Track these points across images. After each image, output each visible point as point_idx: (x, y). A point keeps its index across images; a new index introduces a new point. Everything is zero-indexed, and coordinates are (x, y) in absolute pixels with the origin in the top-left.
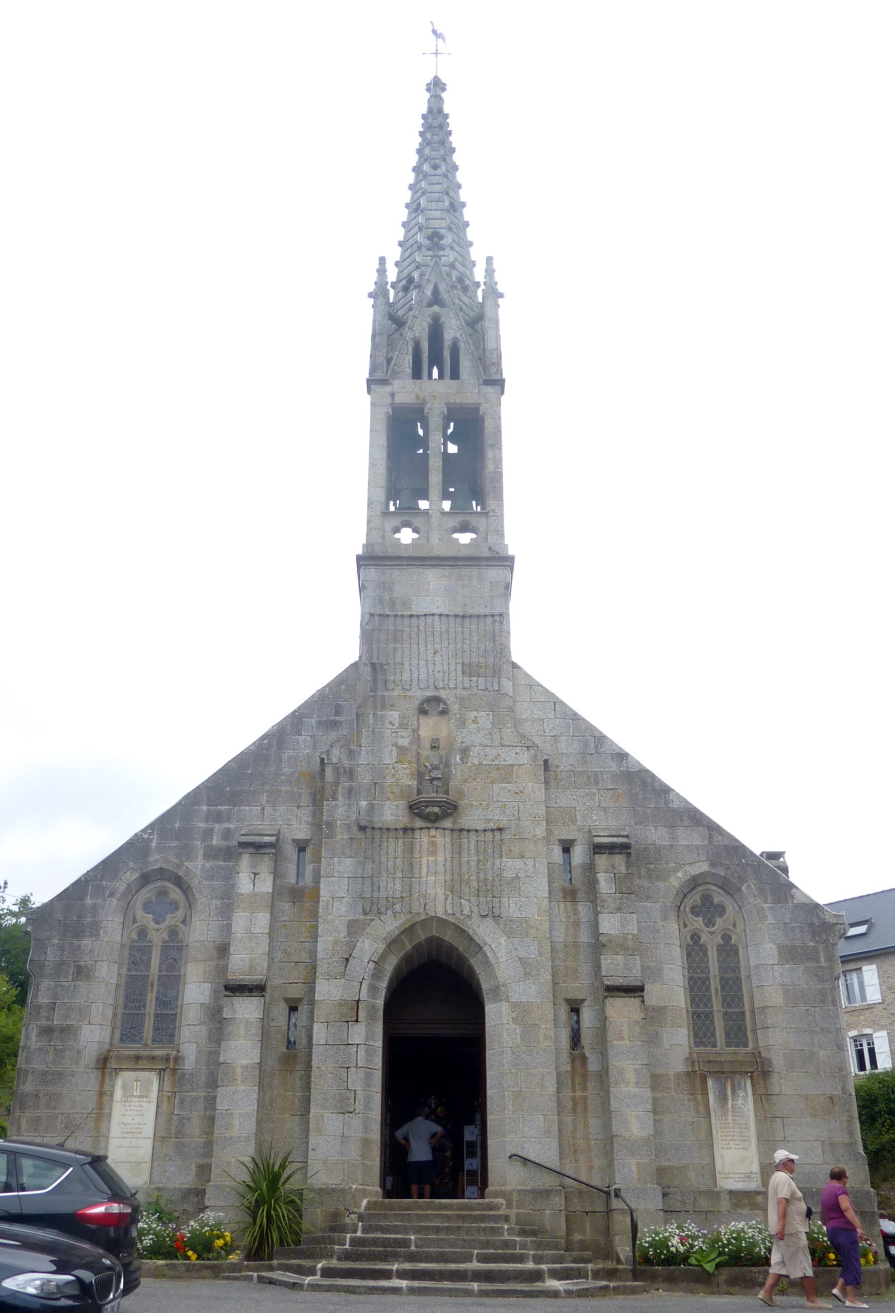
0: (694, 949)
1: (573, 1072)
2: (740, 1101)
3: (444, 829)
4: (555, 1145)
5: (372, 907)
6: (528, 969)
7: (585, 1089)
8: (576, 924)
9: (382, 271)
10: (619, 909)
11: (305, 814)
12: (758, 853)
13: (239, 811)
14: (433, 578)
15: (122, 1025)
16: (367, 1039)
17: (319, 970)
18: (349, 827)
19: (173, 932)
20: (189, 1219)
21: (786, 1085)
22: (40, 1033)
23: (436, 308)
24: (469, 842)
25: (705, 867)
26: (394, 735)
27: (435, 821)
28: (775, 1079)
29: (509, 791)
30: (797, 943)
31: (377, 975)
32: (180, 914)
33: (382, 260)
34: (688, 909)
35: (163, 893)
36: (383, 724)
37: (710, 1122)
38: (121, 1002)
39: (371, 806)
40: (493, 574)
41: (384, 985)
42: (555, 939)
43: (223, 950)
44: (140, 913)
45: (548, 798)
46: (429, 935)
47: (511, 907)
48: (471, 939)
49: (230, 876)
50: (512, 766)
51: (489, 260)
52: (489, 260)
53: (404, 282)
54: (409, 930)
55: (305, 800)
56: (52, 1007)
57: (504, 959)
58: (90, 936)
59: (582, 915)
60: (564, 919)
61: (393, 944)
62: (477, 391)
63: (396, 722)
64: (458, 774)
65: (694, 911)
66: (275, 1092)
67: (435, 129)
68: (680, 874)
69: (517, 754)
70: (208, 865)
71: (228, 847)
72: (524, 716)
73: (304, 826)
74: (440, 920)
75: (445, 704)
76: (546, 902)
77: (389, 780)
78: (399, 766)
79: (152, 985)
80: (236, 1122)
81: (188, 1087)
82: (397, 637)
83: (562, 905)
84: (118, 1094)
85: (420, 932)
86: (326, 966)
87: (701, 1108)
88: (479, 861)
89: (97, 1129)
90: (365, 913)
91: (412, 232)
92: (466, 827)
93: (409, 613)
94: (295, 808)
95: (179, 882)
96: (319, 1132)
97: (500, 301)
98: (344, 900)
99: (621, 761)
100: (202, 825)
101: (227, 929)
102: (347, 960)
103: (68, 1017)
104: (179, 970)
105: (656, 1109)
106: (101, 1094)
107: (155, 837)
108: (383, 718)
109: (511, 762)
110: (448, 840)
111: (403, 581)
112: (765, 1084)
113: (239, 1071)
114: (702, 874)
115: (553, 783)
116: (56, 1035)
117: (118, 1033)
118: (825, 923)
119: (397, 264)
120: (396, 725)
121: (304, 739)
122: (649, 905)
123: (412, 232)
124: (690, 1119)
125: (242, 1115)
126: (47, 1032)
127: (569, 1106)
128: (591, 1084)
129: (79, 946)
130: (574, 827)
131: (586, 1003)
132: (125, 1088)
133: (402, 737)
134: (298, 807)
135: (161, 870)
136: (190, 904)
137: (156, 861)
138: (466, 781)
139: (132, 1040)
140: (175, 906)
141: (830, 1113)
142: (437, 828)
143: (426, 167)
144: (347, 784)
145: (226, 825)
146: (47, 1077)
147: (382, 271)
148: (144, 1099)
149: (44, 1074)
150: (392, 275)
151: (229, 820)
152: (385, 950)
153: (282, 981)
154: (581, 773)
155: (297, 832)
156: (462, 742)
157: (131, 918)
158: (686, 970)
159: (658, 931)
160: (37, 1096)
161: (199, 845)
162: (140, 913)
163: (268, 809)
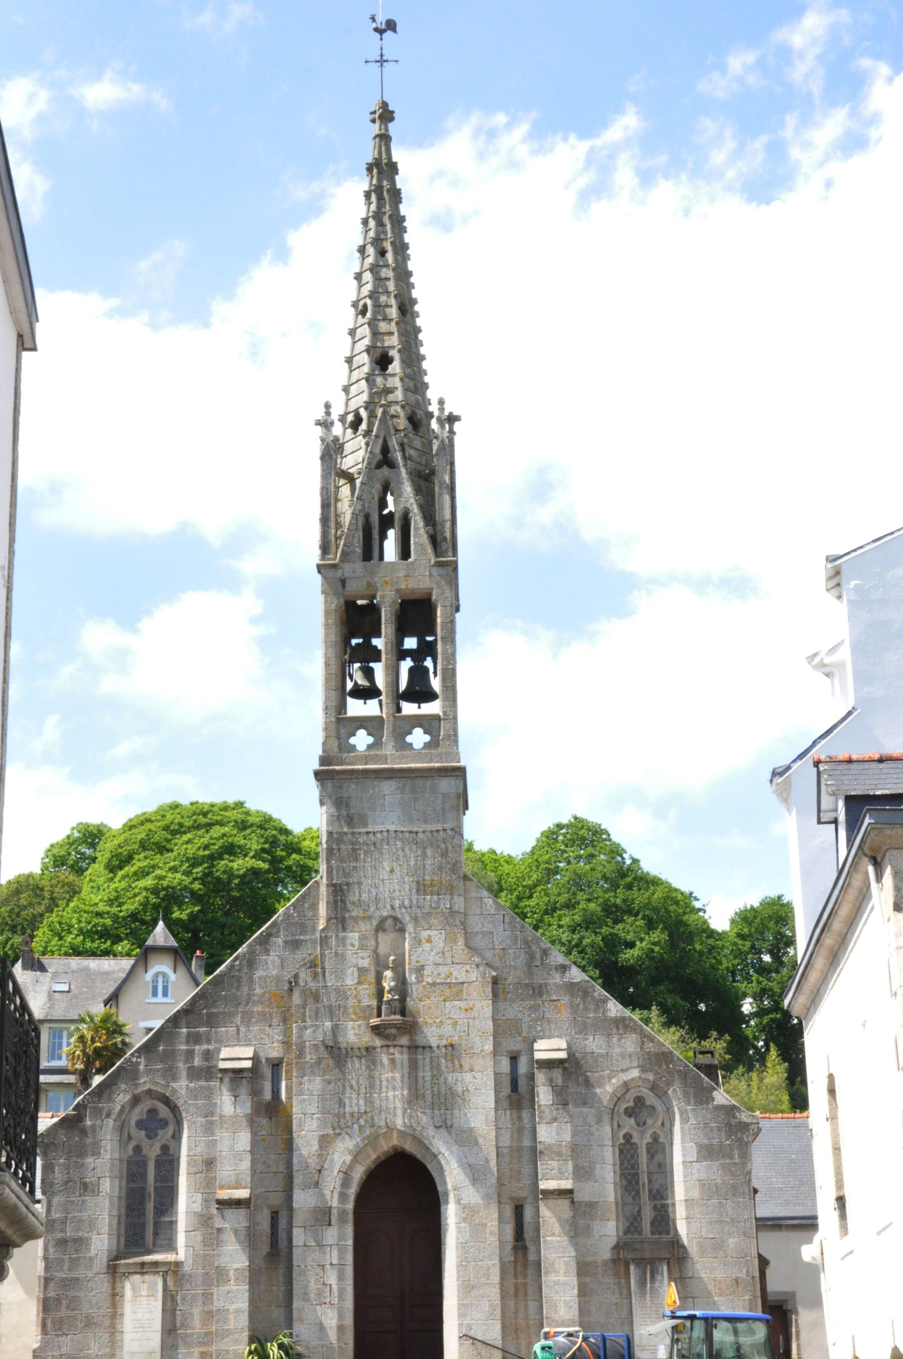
0: (627, 1151)
1: (515, 1261)
2: (657, 1284)
3: (402, 1046)
4: (498, 1327)
5: (338, 1123)
7: (525, 1276)
8: (520, 1131)
10: (555, 1119)
13: (216, 1032)
15: (126, 1232)
16: (339, 1240)
17: (296, 1181)
19: (165, 1148)
20: (690, 1025)
22: (56, 1244)
23: (385, 470)
24: (424, 1059)
26: (355, 956)
29: (460, 1008)
30: (715, 1142)
32: (170, 1130)
34: (622, 1110)
35: (153, 1112)
37: (631, 1302)
38: (123, 1211)
40: (446, 785)
41: (353, 1191)
42: (501, 1144)
43: (210, 1163)
44: (134, 1131)
45: (495, 1011)
46: (391, 1145)
48: (428, 1149)
49: (209, 1094)
50: (463, 983)
51: (441, 402)
53: (350, 417)
56: (64, 1222)
58: (93, 1155)
59: (526, 1121)
60: (510, 1126)
62: (428, 573)
63: (357, 944)
65: (629, 1113)
66: (263, 1287)
68: (614, 1081)
69: (467, 971)
70: (192, 1085)
72: (475, 930)
73: (275, 1045)
75: (401, 923)
76: (493, 1113)
77: (352, 1002)
79: (149, 1195)
80: (232, 1317)
83: (508, 1113)
85: (383, 1142)
86: (301, 1177)
87: (625, 1291)
88: (433, 1076)
89: (113, 1326)
92: (422, 1044)
93: (365, 830)
94: (267, 1028)
95: (166, 1101)
96: (301, 1320)
98: (315, 1116)
99: (564, 972)
100: (183, 1047)
103: (78, 1230)
104: (172, 1181)
105: (583, 1292)
106: (114, 1295)
107: (143, 1060)
108: (344, 938)
109: (462, 980)
112: (680, 1269)
113: (231, 1273)
114: (633, 1079)
115: (501, 996)
117: (122, 1240)
118: (741, 1122)
120: (357, 946)
121: (273, 958)
122: (585, 1110)
124: (614, 1300)
127: (512, 1291)
128: (531, 1272)
129: (83, 1165)
130: (520, 1039)
131: (528, 1201)
132: (134, 1289)
133: (363, 958)
136: (179, 1123)
139: (136, 1245)
140: (164, 1123)
142: (395, 1046)
145: (205, 1047)
148: (151, 1298)
149: (62, 1280)
151: (208, 1041)
152: (352, 1161)
153: (264, 1190)
154: (527, 985)
155: (270, 1050)
156: (418, 962)
157: (126, 1134)
158: (618, 1167)
159: (592, 1134)
160: (58, 1300)
161: (182, 1066)
162: (134, 1131)
163: (242, 1029)
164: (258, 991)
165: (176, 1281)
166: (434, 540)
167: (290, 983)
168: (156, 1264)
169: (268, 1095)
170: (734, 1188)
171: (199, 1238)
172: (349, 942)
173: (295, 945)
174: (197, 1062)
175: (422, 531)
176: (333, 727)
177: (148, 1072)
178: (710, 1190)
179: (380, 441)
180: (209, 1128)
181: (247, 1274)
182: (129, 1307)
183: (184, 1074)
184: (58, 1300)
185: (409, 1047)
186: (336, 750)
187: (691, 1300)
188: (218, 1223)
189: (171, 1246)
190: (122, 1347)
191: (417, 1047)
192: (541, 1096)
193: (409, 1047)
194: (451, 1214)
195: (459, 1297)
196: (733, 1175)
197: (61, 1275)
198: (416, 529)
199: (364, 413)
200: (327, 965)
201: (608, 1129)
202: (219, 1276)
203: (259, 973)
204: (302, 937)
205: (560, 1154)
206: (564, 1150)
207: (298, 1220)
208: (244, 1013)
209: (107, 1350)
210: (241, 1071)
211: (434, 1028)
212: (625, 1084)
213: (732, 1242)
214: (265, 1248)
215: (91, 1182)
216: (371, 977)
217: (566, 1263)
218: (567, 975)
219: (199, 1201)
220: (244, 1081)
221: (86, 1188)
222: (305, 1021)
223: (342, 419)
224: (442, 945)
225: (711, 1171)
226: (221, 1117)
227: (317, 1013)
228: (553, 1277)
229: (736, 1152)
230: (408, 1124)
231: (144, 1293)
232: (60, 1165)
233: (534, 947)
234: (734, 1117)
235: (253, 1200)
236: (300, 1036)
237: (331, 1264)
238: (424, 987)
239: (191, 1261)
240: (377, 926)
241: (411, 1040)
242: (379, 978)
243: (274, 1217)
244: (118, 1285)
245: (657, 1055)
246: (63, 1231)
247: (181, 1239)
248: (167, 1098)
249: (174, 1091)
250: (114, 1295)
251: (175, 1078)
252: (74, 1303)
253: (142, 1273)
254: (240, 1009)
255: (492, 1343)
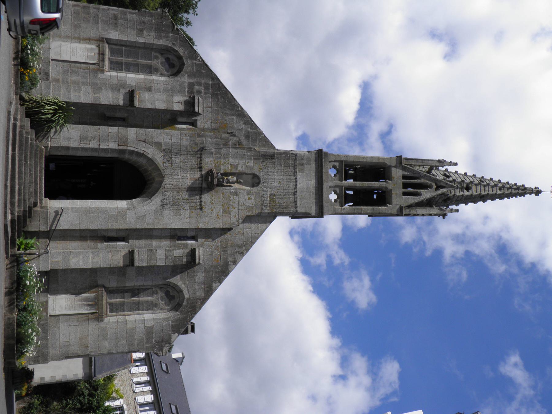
2: (86, 307)
3: (202, 184)
5: (168, 152)
6: (141, 218)
9: (450, 164)
10: (167, 257)
11: (208, 125)
12: (193, 321)
14: (312, 183)
18: (202, 143)
21: (92, 327)
23: (435, 187)
25: (187, 296)
27: (205, 180)
28: (95, 323)
30: (154, 335)
31: (138, 154)
33: (456, 164)
34: (168, 289)
36: (248, 159)
39: (212, 153)
43: (149, 89)
47: (167, 213)
49: (181, 92)
50: (230, 214)
51: (457, 211)
52: (457, 211)
53: (448, 174)
54: (157, 168)
55: (214, 125)
56: (125, 19)
57: (145, 208)
61: (151, 161)
63: (249, 165)
64: (225, 190)
67: (519, 191)
68: (183, 286)
71: (194, 93)
74: (162, 181)
77: (223, 161)
78: (229, 166)
80: (77, 94)
81: (91, 75)
82: (287, 165)
83: (169, 234)
84: (89, 46)
90: (165, 150)
91: (461, 177)
97: (441, 217)
99: (233, 262)
100: (203, 81)
101: (158, 91)
102: (145, 142)
104: (141, 72)
106: (89, 39)
108: (251, 159)
109: (231, 213)
110: (197, 186)
111: (311, 168)
113: (98, 95)
114: (184, 295)
116: (114, 21)
119: (456, 172)
121: (242, 126)
122: (170, 272)
123: (461, 177)
125: (79, 96)
126: (115, 18)
129: (151, 31)
132: (92, 49)
134: (211, 123)
135: (184, 64)
137: (188, 62)
138: (223, 194)
141: (81, 345)
142: (202, 181)
143: (500, 185)
144: (221, 143)
145: (203, 91)
146: (96, 17)
147: (450, 164)
149: (98, 16)
150: (452, 169)
151: (205, 93)
152: (149, 158)
154: (227, 244)
160: (88, 13)
161: (194, 80)
163: (210, 109)
164: (227, 118)
165: (94, 70)
166: (410, 207)
167: (232, 133)
168: (103, 61)
169: (180, 119)
170: (132, 345)
171: (114, 82)
172: (249, 161)
173: (247, 136)
174: (196, 87)
175: (413, 201)
176: (339, 159)
177: (193, 64)
178: (131, 333)
179: (444, 185)
180: (165, 90)
181: (97, 103)
182: (82, 46)
183: (191, 81)
184: (88, 13)
185: (201, 187)
186: (330, 160)
187: (78, 324)
188: (123, 91)
189: (112, 69)
190: (64, 41)
191: (201, 191)
192: (178, 251)
193: (201, 187)
194: (122, 204)
195: (82, 208)
196: (138, 344)
197: (100, 16)
198: (414, 199)
199: (451, 179)
200: (239, 150)
201: (160, 283)
202: (97, 88)
203: (235, 118)
204: (250, 140)
205: (150, 259)
206: (152, 262)
207: (122, 130)
208: (218, 110)
209: (63, 34)
210: (194, 107)
211: (210, 199)
212: (182, 291)
213: (106, 344)
214: (108, 114)
215: (143, 34)
216: (234, 171)
217: (98, 262)
218: (232, 263)
219: (131, 84)
220: (188, 108)
221: (140, 32)
222: (214, 138)
223: (446, 170)
224: (247, 205)
225: (140, 334)
226: (172, 96)
227: (218, 144)
228: (91, 255)
229: (149, 345)
230: (166, 186)
231: (89, 54)
232: (152, 20)
233: (244, 248)
234: (166, 344)
235: (132, 108)
236: (208, 136)
237: (100, 145)
238: (229, 196)
239: (104, 77)
240: (256, 175)
241: (205, 189)
242: (233, 174)
243: (124, 119)
244: (94, 42)
245: (195, 306)
246: (121, 19)
247: (114, 74)
248: (180, 72)
249: (184, 75)
250: (89, 39)
251: (189, 76)
252: (87, 20)
253: (99, 54)
254: (220, 109)
255: (58, 224)
